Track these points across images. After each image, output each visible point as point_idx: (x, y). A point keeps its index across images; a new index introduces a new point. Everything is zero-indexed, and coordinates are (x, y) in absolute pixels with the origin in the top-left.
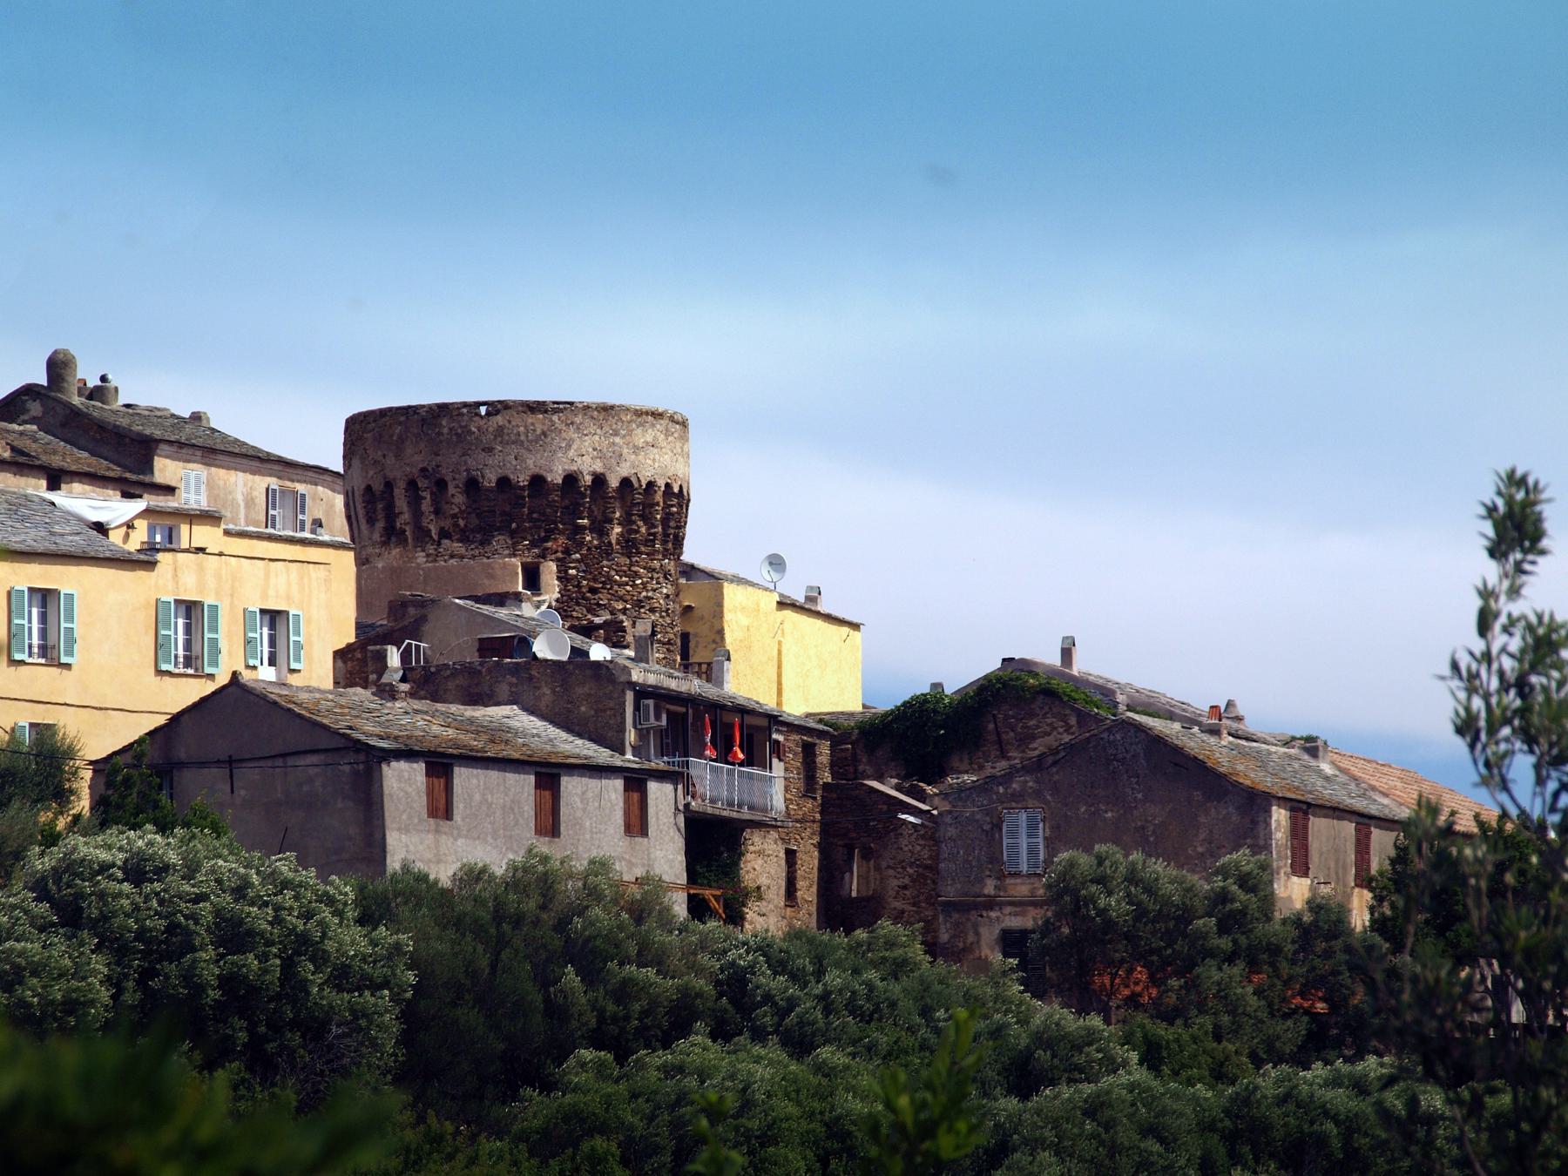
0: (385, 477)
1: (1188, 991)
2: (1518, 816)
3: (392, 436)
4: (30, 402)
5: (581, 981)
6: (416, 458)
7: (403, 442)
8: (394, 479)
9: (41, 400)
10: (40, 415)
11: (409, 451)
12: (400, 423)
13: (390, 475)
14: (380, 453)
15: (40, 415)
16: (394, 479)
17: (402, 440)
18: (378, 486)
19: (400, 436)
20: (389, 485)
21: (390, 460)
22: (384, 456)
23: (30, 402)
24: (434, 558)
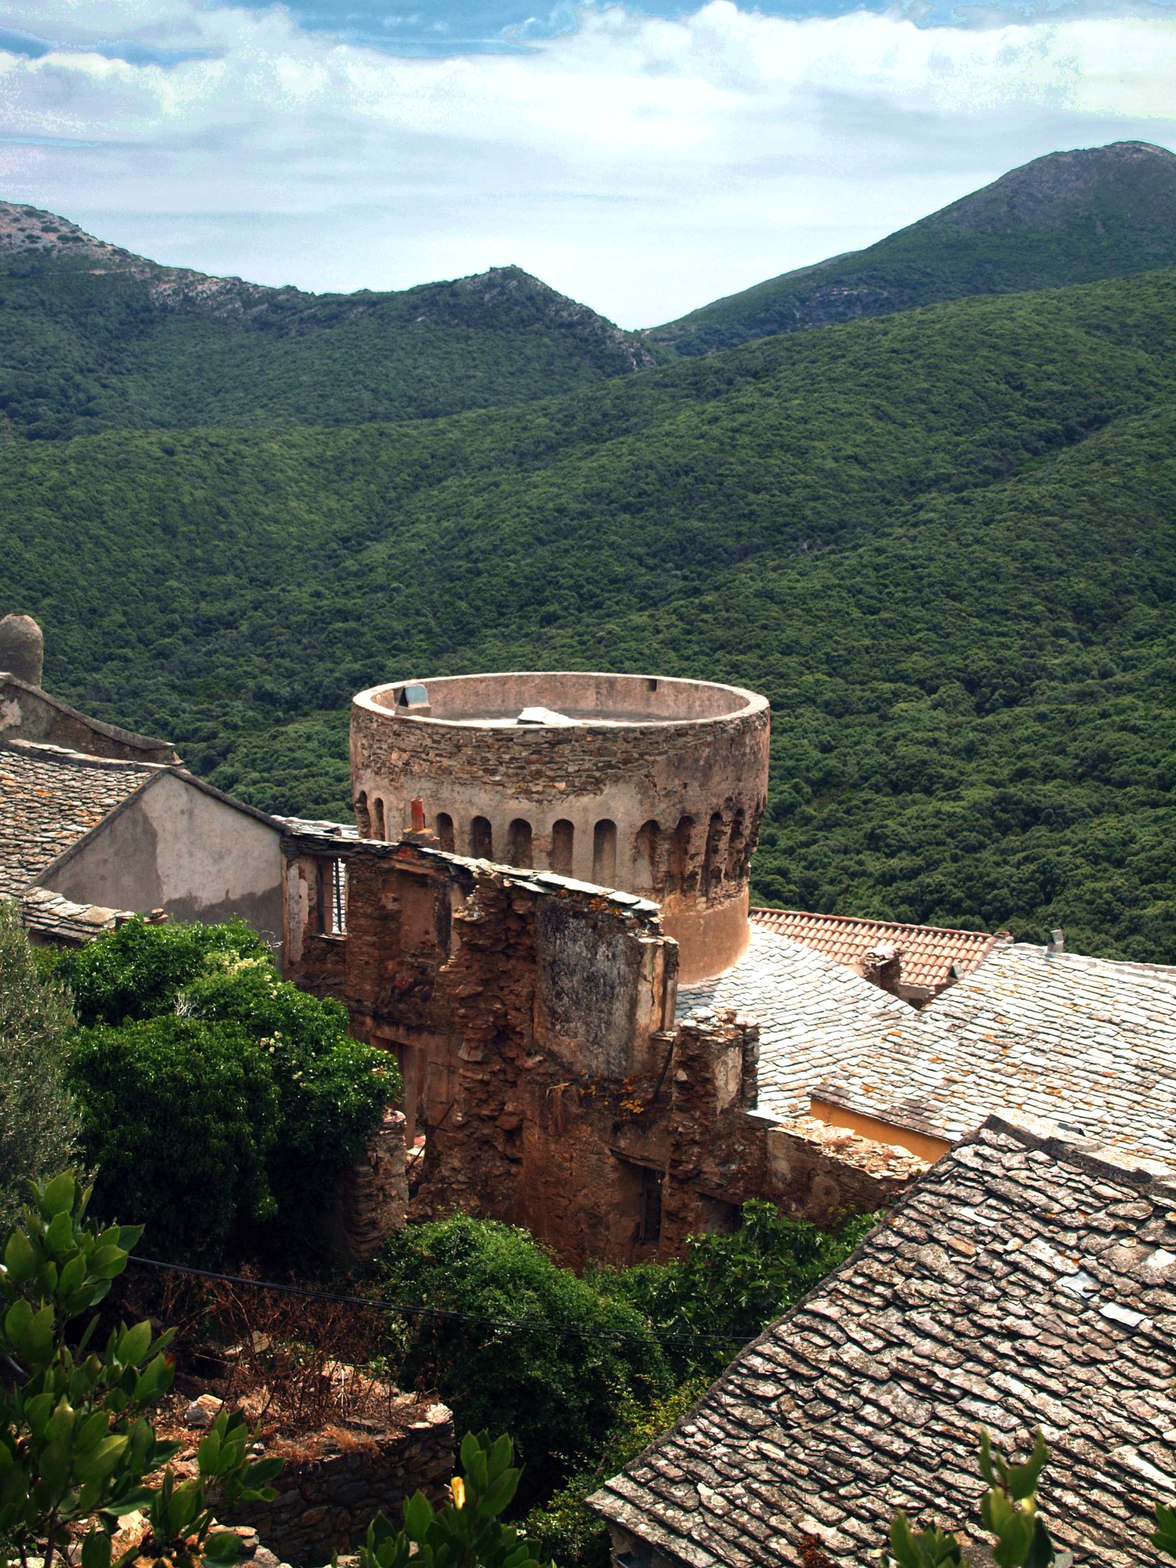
0: (683, 811)
1: (24, 1111)
2: (643, 1064)
3: (697, 760)
4: (7, 703)
5: (535, 1235)
6: (724, 786)
7: (710, 767)
8: (697, 814)
9: (19, 699)
10: (19, 722)
11: (716, 779)
12: (709, 745)
13: (692, 809)
14: (677, 782)
15: (19, 722)
16: (697, 814)
17: (709, 765)
18: (668, 823)
19: (707, 761)
20: (687, 821)
21: (694, 790)
22: (685, 786)
23: (7, 703)
24: (711, 902)
